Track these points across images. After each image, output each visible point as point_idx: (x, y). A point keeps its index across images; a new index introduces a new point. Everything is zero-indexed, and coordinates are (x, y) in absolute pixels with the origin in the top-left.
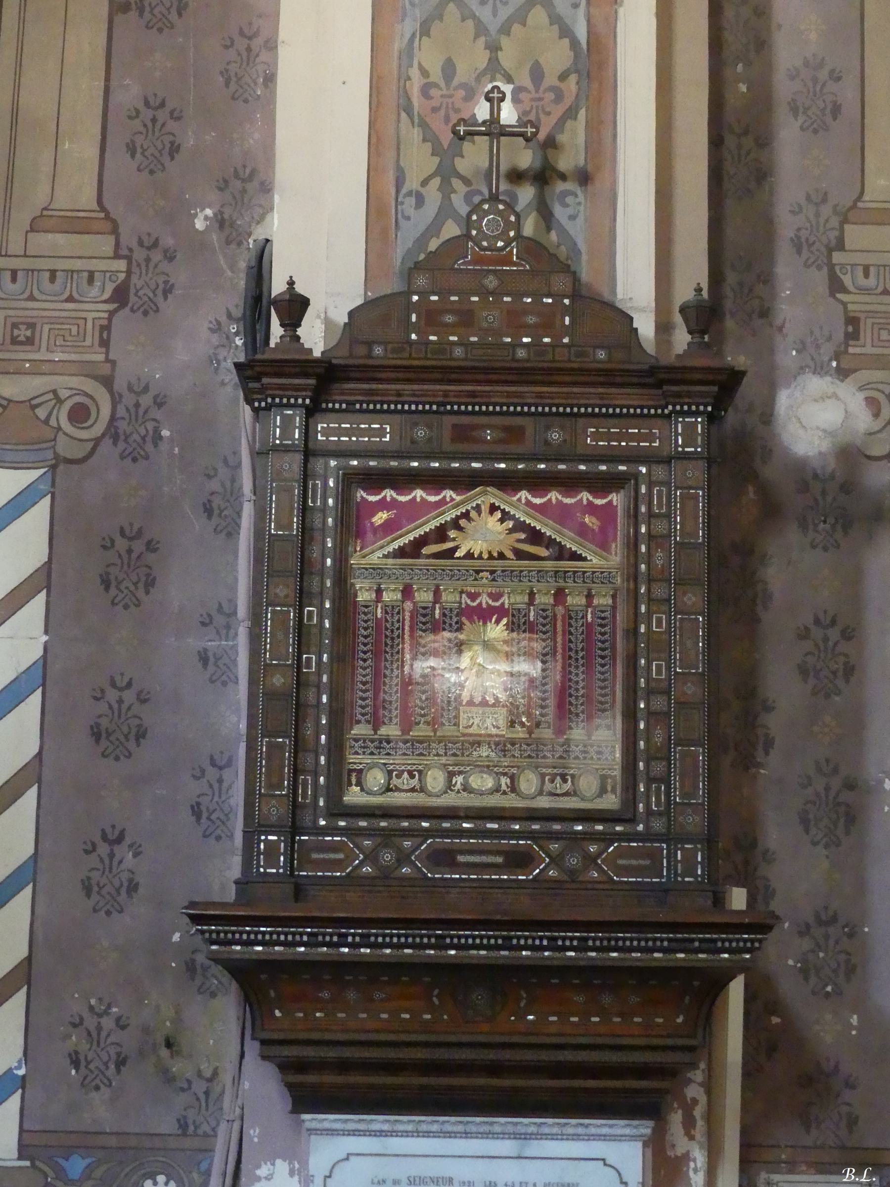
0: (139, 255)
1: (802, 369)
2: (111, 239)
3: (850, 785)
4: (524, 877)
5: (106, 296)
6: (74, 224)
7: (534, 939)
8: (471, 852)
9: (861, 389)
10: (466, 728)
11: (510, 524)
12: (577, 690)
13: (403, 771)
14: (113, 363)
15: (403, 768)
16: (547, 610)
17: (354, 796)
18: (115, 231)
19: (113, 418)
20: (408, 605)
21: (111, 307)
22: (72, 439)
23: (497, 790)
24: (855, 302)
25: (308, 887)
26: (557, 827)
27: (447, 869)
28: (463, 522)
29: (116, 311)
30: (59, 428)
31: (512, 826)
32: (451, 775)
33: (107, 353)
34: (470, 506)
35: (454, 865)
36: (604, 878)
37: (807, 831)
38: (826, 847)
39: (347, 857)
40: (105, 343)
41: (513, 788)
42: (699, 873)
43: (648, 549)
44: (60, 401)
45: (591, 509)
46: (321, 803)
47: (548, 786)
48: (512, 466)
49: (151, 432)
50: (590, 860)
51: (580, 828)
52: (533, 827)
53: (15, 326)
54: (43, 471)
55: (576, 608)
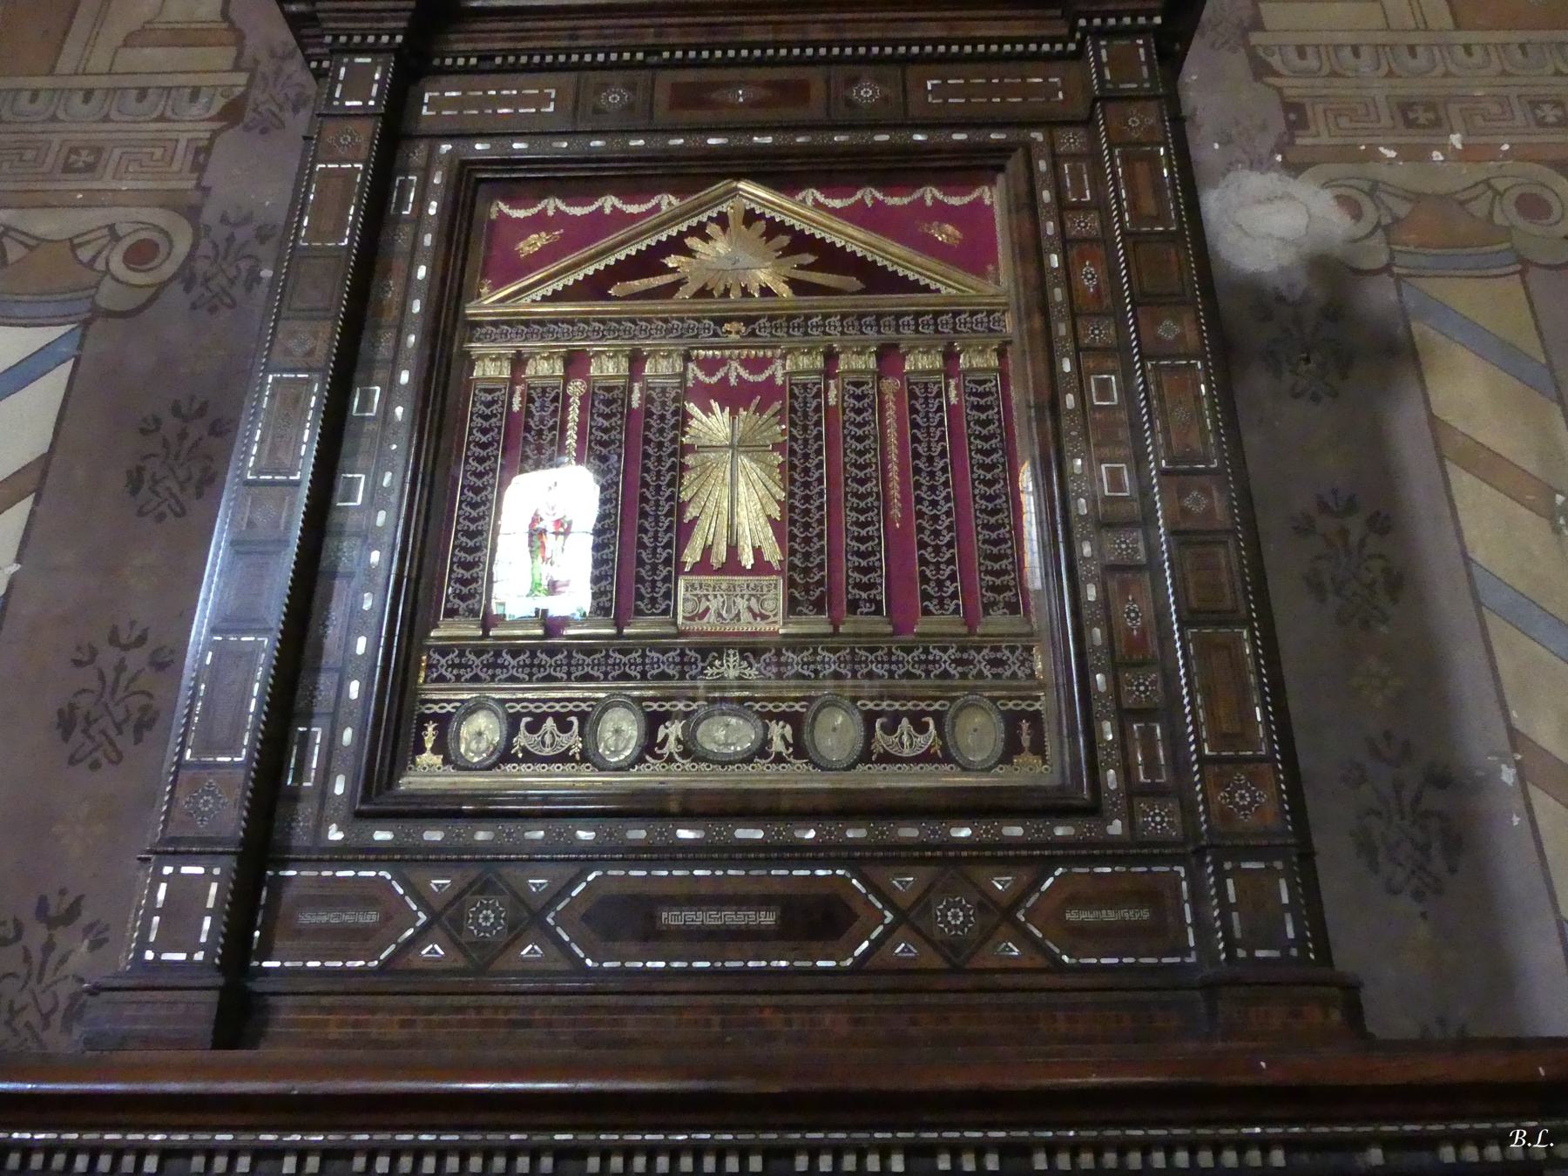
0: (266, 66)
1: (1230, 166)
2: (232, 52)
3: (1442, 779)
4: (831, 964)
5: (213, 112)
6: (181, 37)
7: (862, 1155)
8: (695, 900)
9: (1325, 186)
10: (691, 619)
11: (785, 240)
12: (936, 534)
13: (544, 716)
14: (206, 191)
15: (545, 708)
16: (863, 384)
17: (427, 773)
18: (240, 39)
19: (191, 256)
20: (576, 388)
21: (216, 125)
22: (122, 281)
23: (762, 750)
24: (1294, 88)
25: (272, 1000)
26: (909, 832)
27: (634, 948)
28: (693, 242)
29: (222, 130)
30: (107, 271)
31: (798, 834)
32: (653, 721)
33: (199, 179)
34: (709, 213)
35: (653, 937)
36: (1040, 961)
37: (1374, 867)
38: (1418, 895)
39: (387, 918)
40: (199, 168)
41: (799, 749)
42: (1291, 934)
43: (1064, 260)
44: (115, 238)
45: (943, 213)
46: (339, 789)
47: (882, 741)
48: (783, 139)
49: (244, 274)
50: (998, 914)
51: (965, 832)
52: (850, 834)
53: (75, 150)
54: (69, 327)
55: (925, 379)
